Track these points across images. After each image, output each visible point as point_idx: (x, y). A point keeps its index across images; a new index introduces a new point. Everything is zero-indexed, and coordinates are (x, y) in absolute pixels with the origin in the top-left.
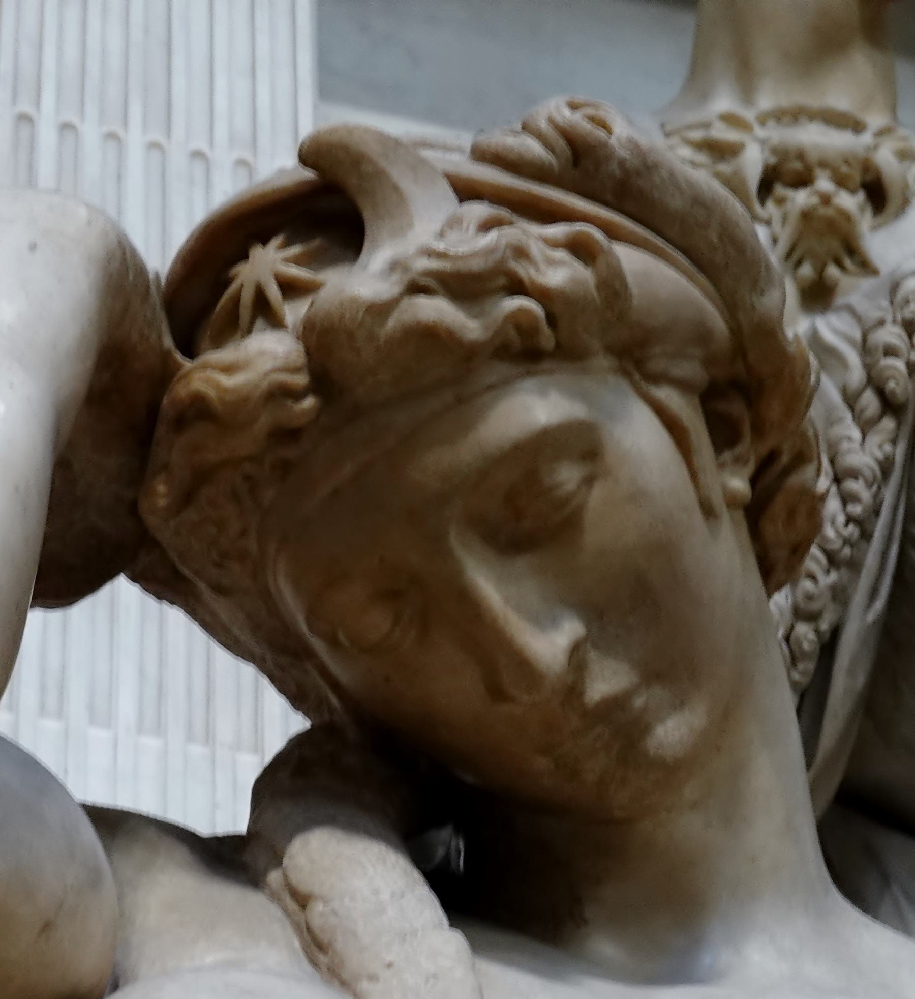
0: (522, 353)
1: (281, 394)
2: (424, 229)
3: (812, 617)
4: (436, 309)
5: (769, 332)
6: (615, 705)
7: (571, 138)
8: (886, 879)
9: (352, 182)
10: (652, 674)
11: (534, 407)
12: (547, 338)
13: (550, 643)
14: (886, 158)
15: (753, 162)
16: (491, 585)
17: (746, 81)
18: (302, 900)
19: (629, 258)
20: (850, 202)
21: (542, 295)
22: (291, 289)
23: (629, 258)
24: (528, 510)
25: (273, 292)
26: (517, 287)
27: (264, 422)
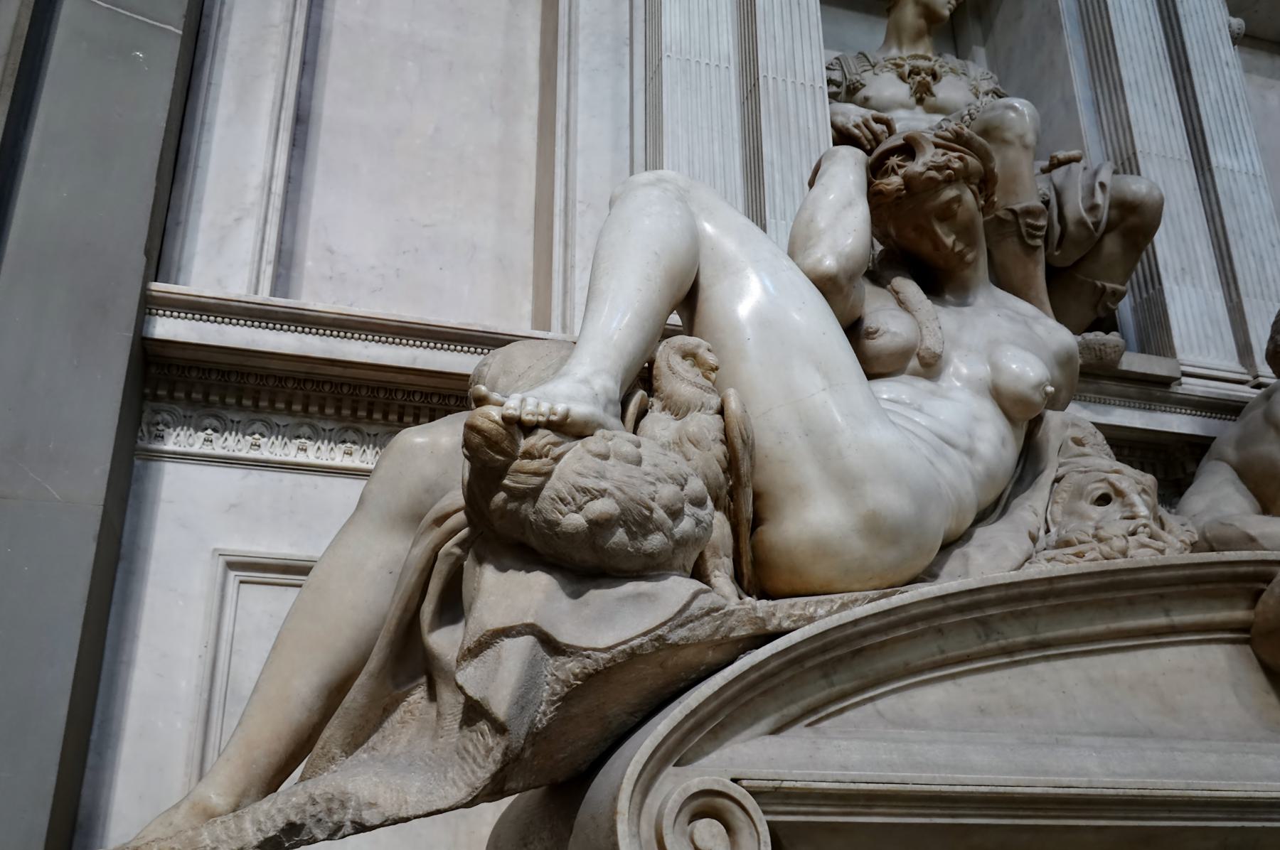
0: (949, 181)
1: (899, 190)
2: (928, 157)
4: (933, 173)
7: (956, 132)
10: (967, 245)
11: (950, 193)
13: (949, 240)
14: (937, 68)
15: (907, 69)
16: (939, 229)
17: (900, 46)
18: (897, 293)
19: (969, 158)
20: (929, 79)
21: (953, 169)
22: (900, 167)
23: (969, 158)
24: (947, 213)
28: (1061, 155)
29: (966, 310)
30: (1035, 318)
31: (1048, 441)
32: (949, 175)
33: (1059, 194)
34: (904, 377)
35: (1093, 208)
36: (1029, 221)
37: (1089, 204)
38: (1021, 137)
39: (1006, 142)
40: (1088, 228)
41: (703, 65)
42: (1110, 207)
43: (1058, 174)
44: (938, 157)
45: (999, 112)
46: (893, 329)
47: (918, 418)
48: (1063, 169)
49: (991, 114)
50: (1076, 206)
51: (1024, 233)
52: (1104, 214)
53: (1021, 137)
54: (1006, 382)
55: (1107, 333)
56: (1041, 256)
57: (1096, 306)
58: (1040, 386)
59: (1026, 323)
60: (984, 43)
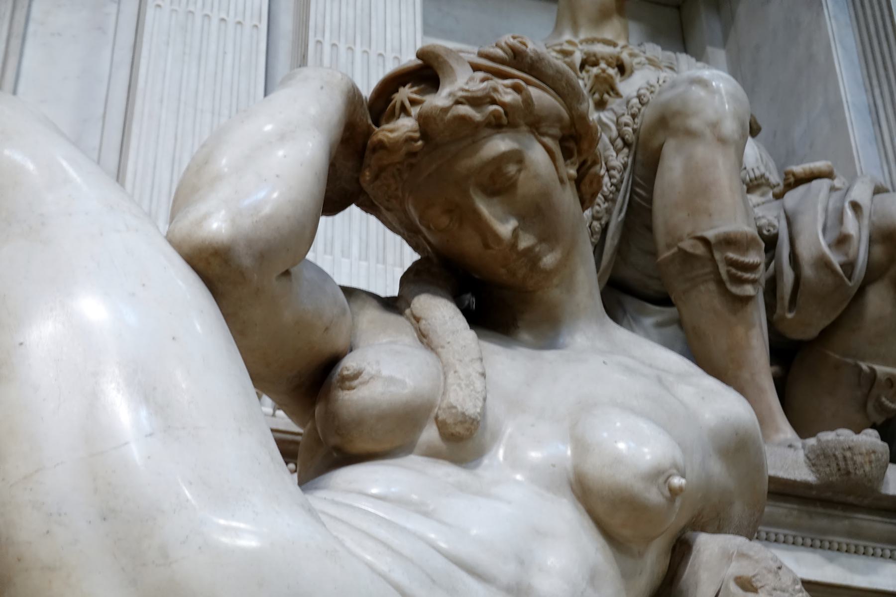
0: (496, 125)
1: (410, 140)
2: (461, 81)
3: (599, 219)
4: (465, 110)
5: (584, 118)
6: (529, 250)
8: (625, 312)
9: (435, 64)
11: (500, 144)
12: (505, 120)
13: (505, 228)
14: (625, 56)
15: (578, 57)
16: (485, 208)
17: (575, 30)
18: (418, 320)
19: (534, 92)
20: (612, 72)
21: (503, 105)
22: (413, 102)
23: (534, 92)
24: (498, 181)
25: (407, 104)
26: (494, 102)
27: (404, 150)
28: (799, 169)
29: (549, 355)
30: (682, 376)
31: (696, 585)
32: (494, 114)
33: (790, 223)
34: (414, 460)
35: (842, 241)
36: (731, 255)
37: (833, 235)
38: (714, 126)
39: (691, 134)
40: (833, 271)
41: (215, 21)
42: (871, 241)
43: (792, 198)
44: (477, 84)
45: (680, 89)
46: (385, 372)
47: (415, 523)
48: (802, 189)
49: (667, 96)
50: (814, 241)
51: (724, 276)
52: (861, 252)
53: (714, 126)
54: (598, 469)
55: (858, 432)
56: (759, 314)
57: (864, 406)
58: (658, 475)
59: (660, 381)
60: (724, 43)
